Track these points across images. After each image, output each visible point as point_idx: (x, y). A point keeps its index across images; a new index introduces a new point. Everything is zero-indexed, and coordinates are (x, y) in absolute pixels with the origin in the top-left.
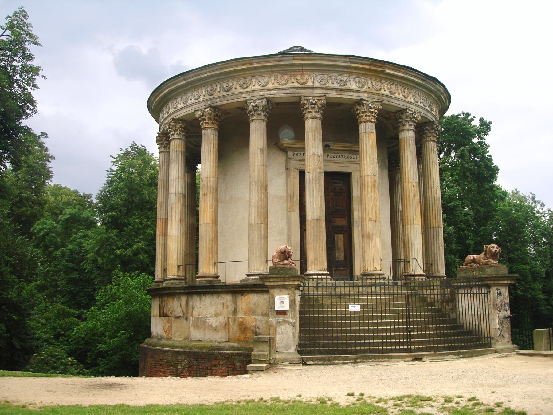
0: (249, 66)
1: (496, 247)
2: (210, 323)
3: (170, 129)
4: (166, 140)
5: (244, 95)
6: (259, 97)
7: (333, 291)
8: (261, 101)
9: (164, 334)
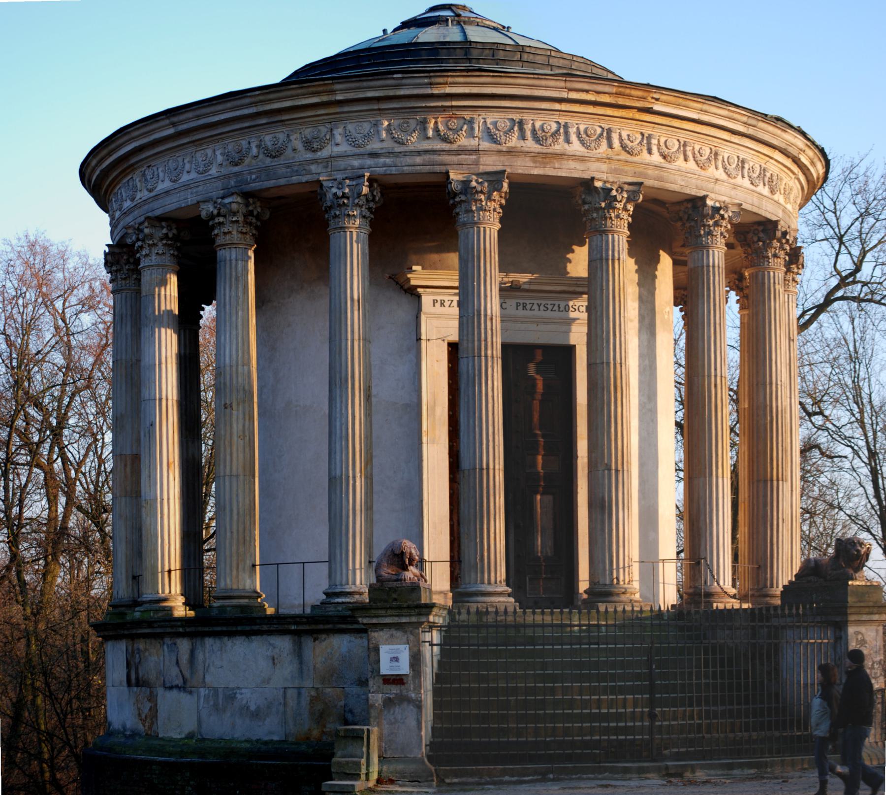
0: (325, 98)
2: (244, 702)
3: (140, 243)
4: (128, 262)
5: (313, 168)
6: (349, 173)
8: (354, 183)
9: (141, 727)
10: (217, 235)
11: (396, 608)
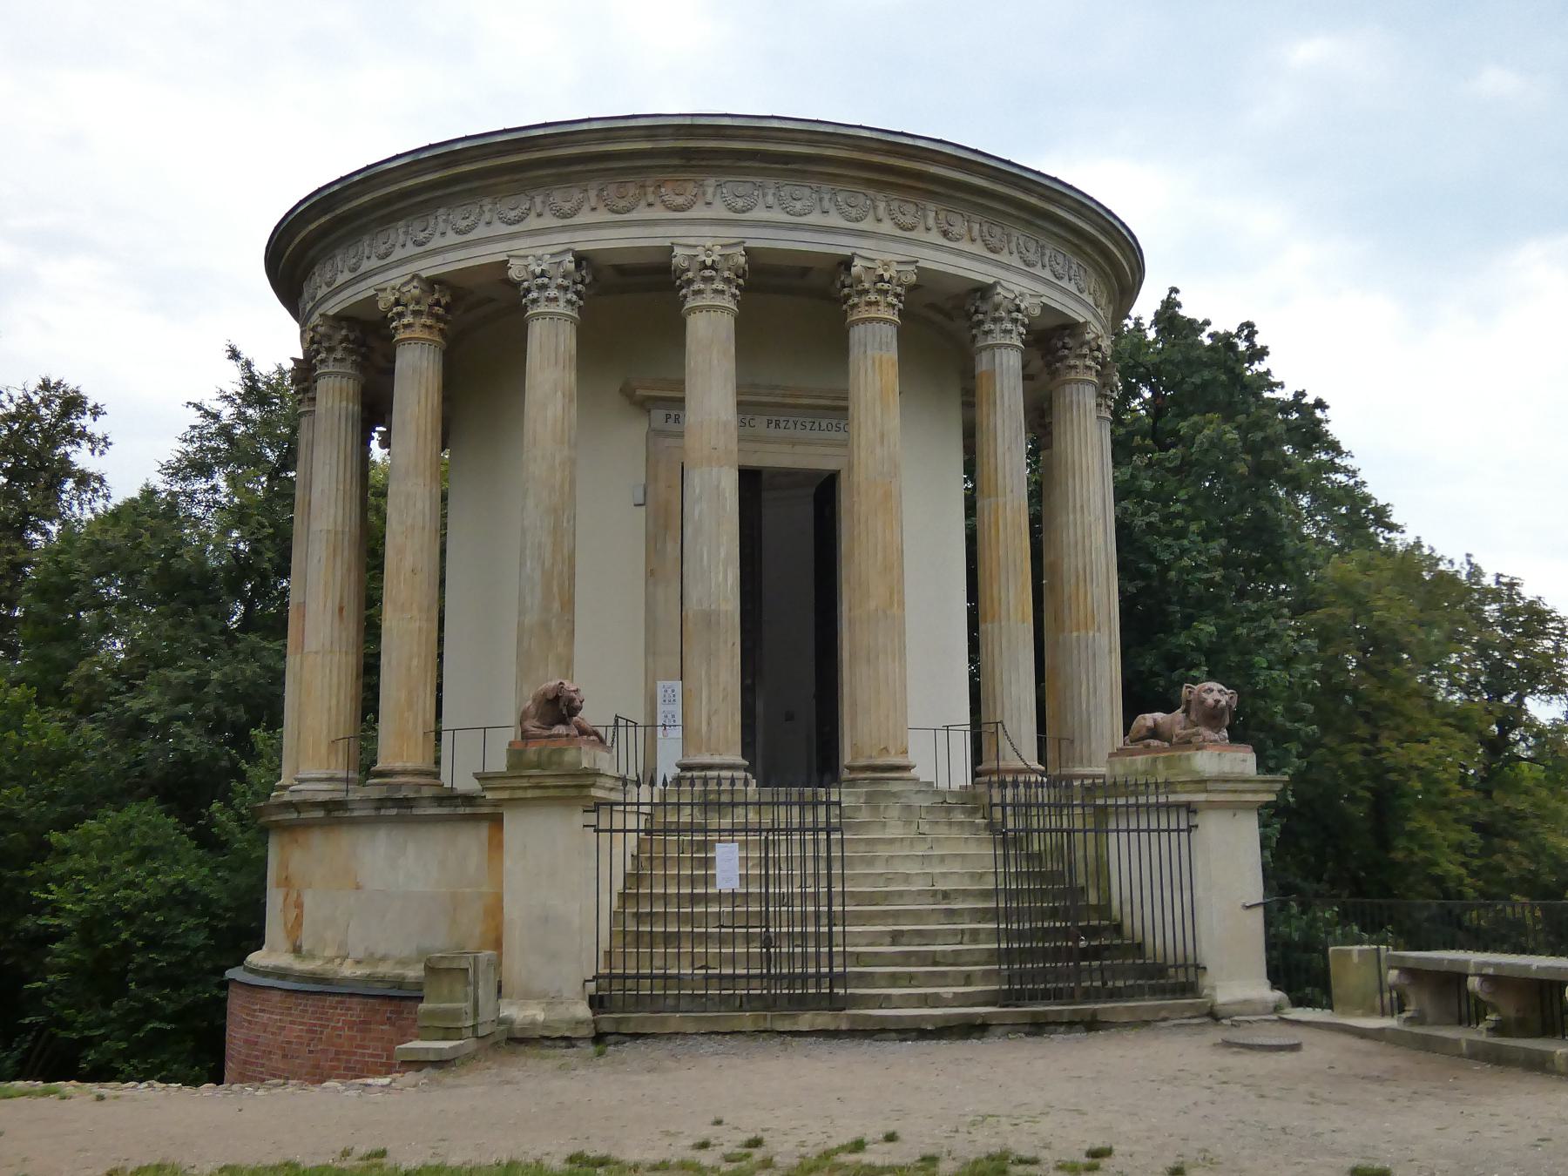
1: (1220, 691)
7: (751, 815)
10: (396, 328)
11: (883, 1031)
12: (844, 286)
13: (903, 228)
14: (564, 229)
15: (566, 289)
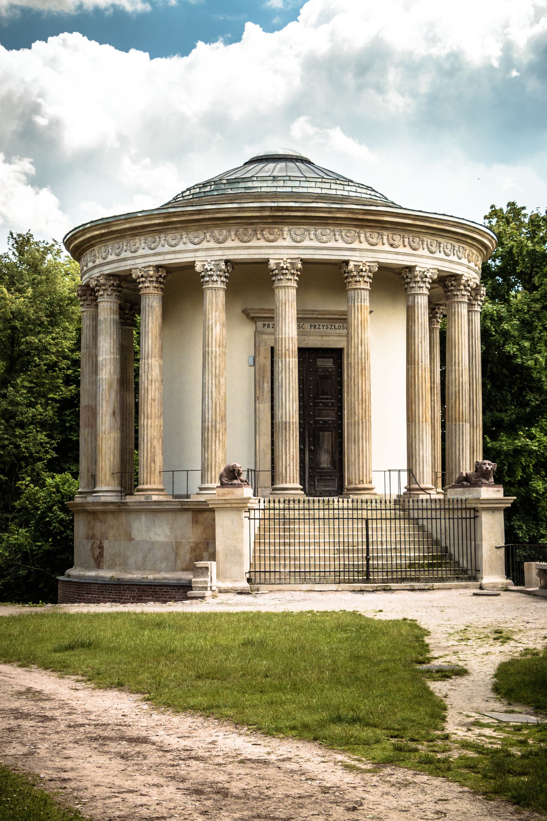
10: (141, 288)
12: (345, 272)
13: (372, 245)
14: (220, 248)
15: (221, 276)
